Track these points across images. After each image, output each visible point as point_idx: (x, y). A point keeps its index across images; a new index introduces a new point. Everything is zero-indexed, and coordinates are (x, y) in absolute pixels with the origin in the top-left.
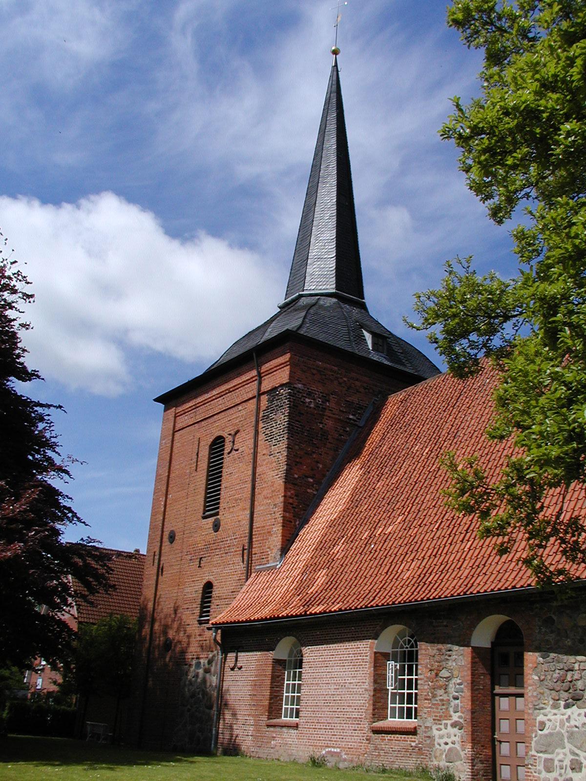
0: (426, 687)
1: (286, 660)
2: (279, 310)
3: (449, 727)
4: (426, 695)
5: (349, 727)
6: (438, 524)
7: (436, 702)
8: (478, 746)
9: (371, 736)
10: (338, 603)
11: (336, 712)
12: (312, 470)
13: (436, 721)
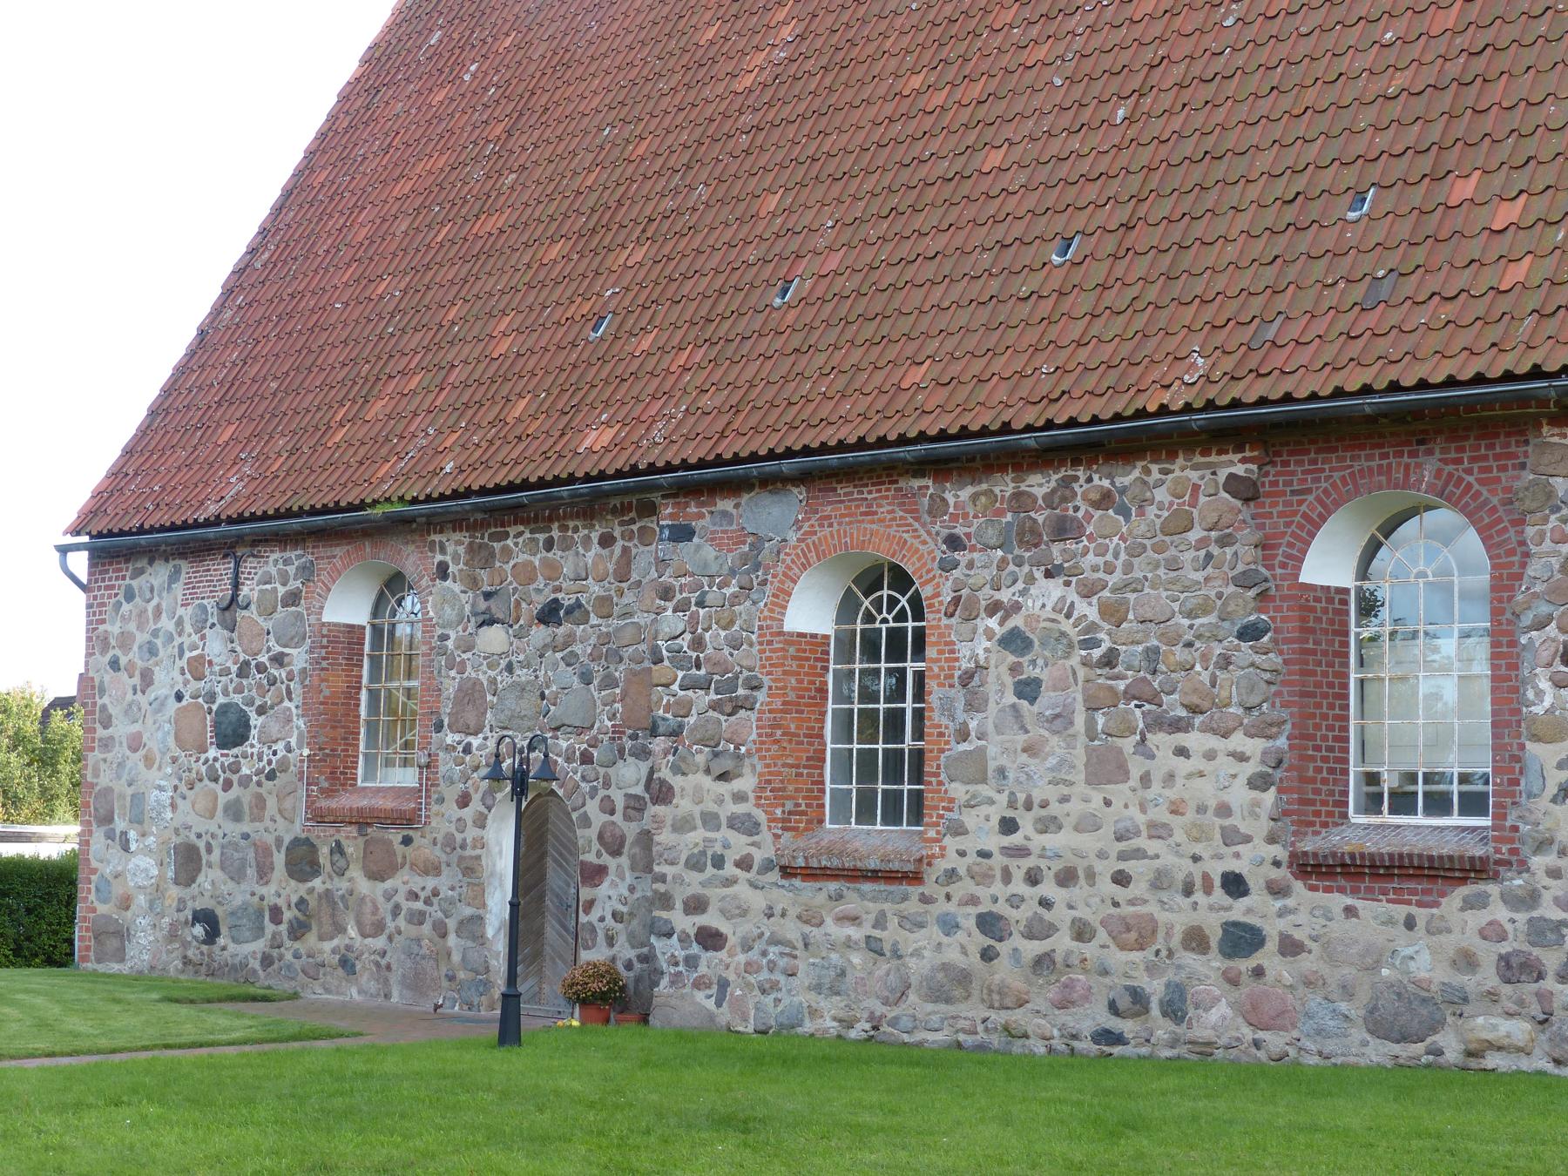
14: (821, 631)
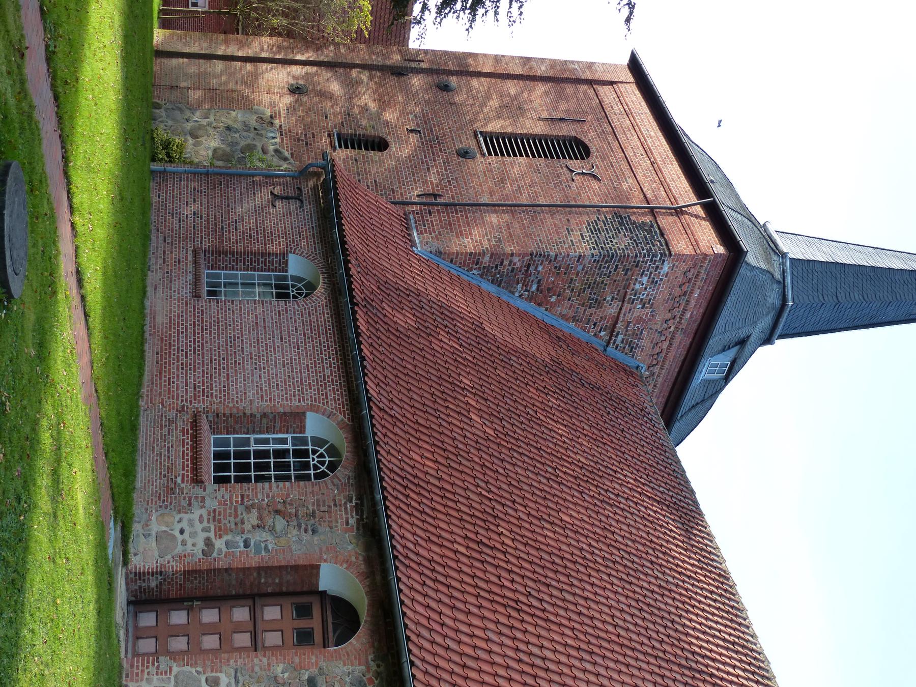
0: (260, 496)
1: (287, 271)
2: (762, 224)
3: (206, 535)
4: (248, 496)
5: (199, 377)
6: (486, 494)
7: (239, 513)
8: (181, 580)
9: (187, 412)
10: (372, 353)
11: (219, 357)
12: (549, 289)
13: (212, 515)
14: (289, 271)
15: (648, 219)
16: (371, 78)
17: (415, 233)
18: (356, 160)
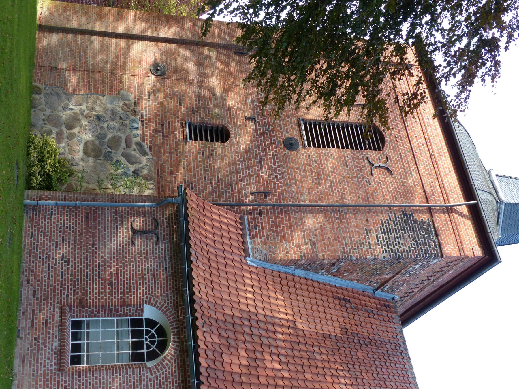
1: (142, 316)
15: (426, 217)
16: (218, 57)
17: (248, 237)
18: (203, 154)
